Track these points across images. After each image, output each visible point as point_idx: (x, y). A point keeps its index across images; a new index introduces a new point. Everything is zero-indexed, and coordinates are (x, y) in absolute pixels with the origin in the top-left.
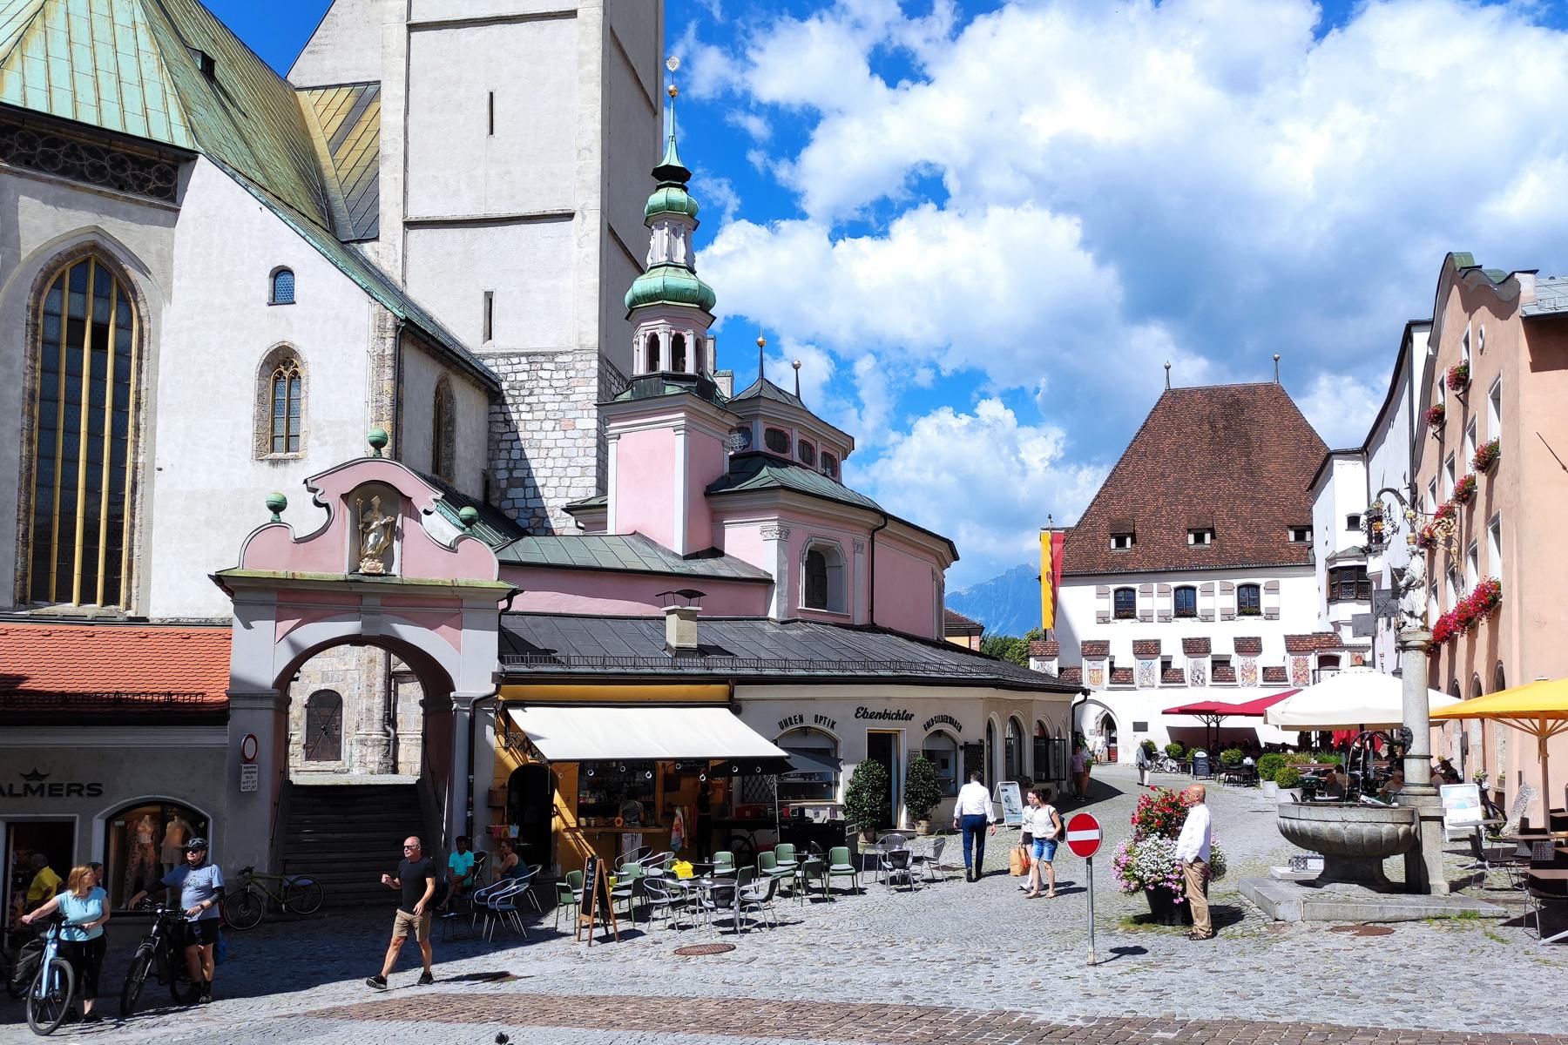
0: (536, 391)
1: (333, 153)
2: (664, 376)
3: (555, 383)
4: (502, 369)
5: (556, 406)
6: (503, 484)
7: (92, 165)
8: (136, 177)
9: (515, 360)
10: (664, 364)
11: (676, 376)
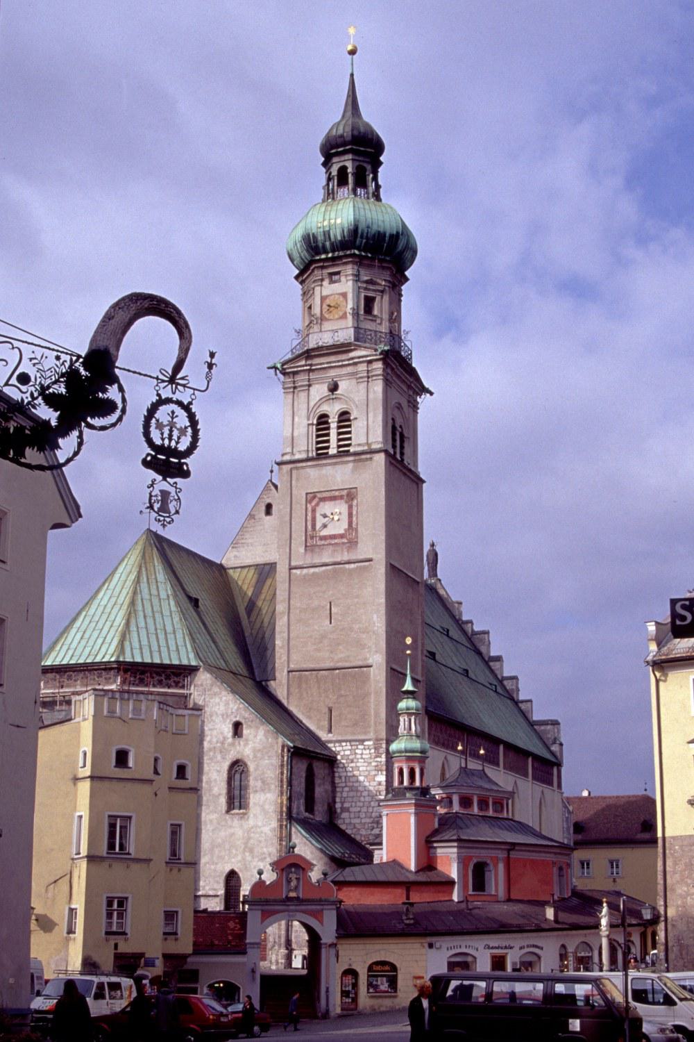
0: (355, 760)
1: (249, 616)
2: (406, 788)
3: (364, 756)
4: (338, 749)
5: (365, 769)
6: (339, 811)
7: (158, 680)
8: (174, 682)
9: (344, 744)
10: (406, 783)
11: (411, 788)
